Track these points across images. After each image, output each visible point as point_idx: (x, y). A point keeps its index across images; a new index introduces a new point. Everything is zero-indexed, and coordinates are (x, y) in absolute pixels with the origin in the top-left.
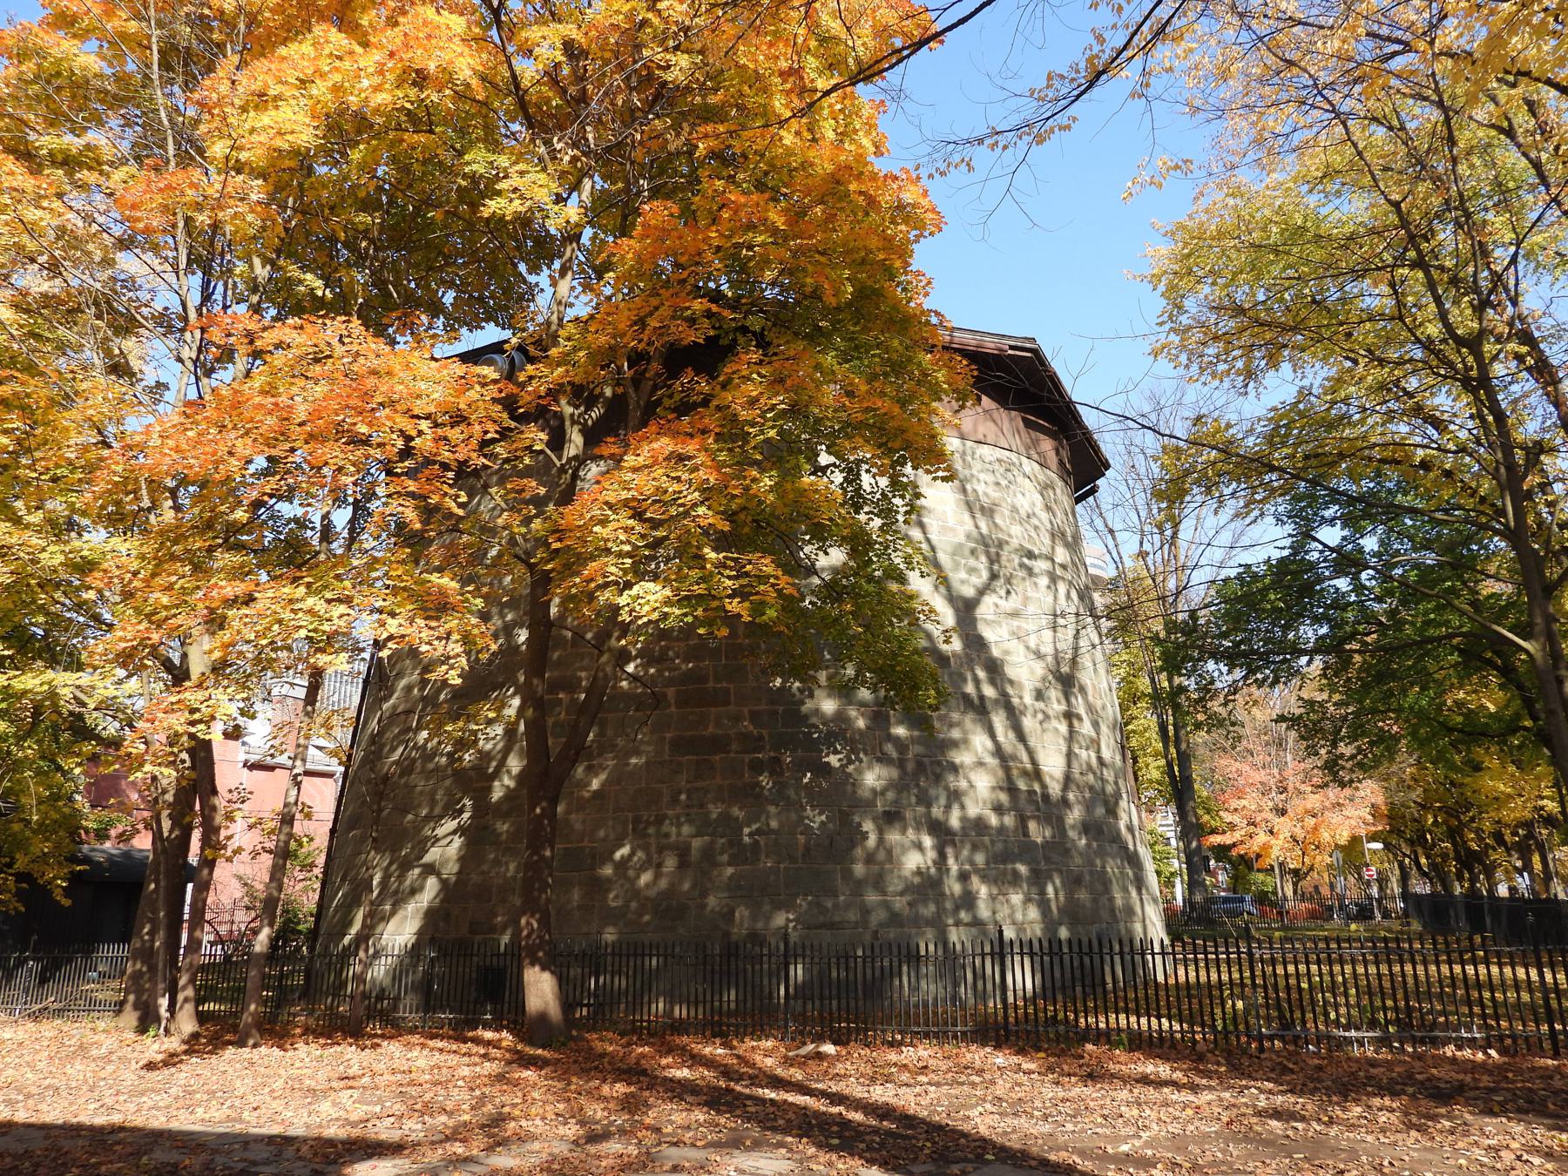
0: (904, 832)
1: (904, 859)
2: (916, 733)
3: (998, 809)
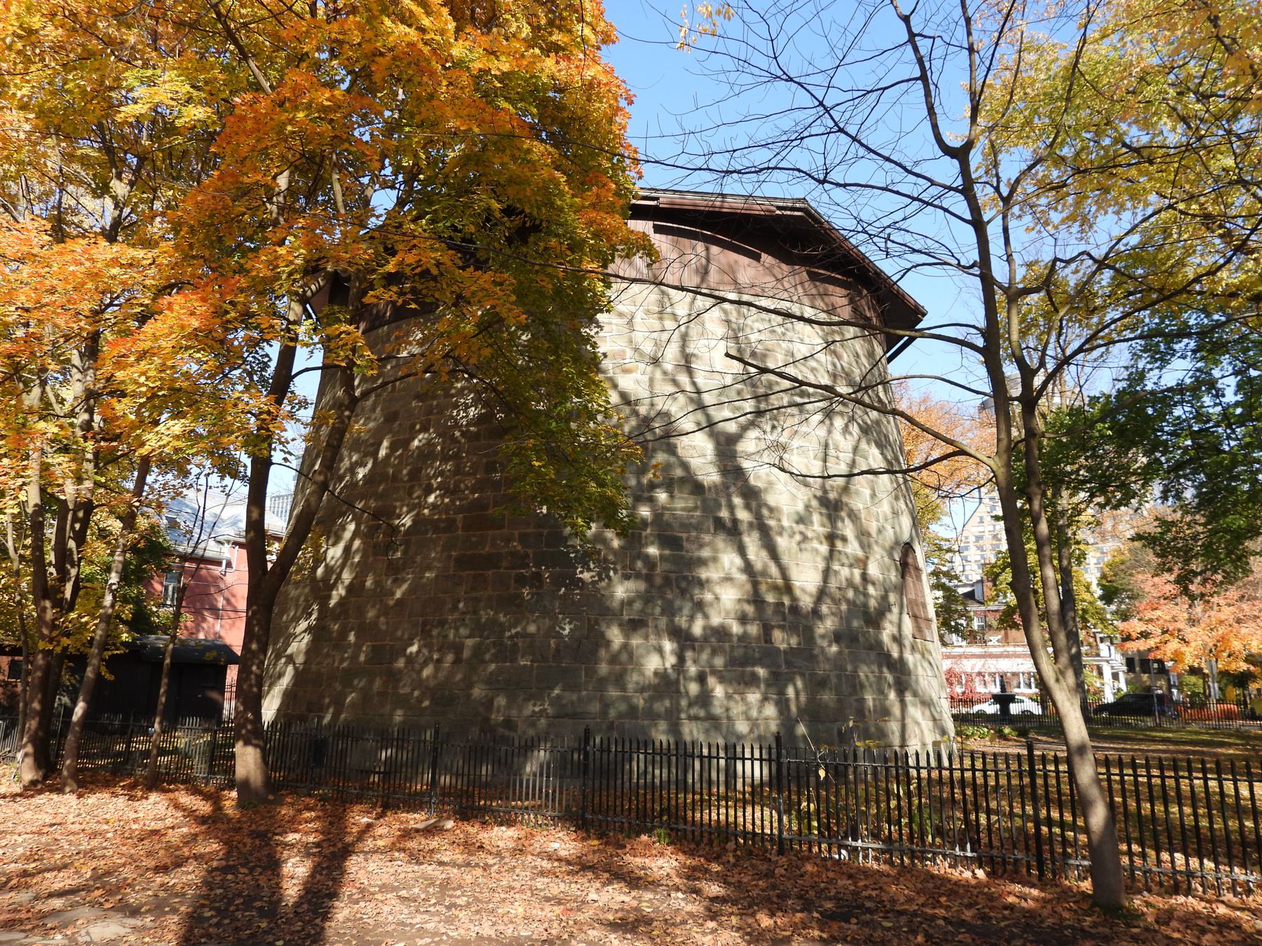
0: (646, 638)
1: (643, 661)
2: (667, 552)
3: (743, 619)
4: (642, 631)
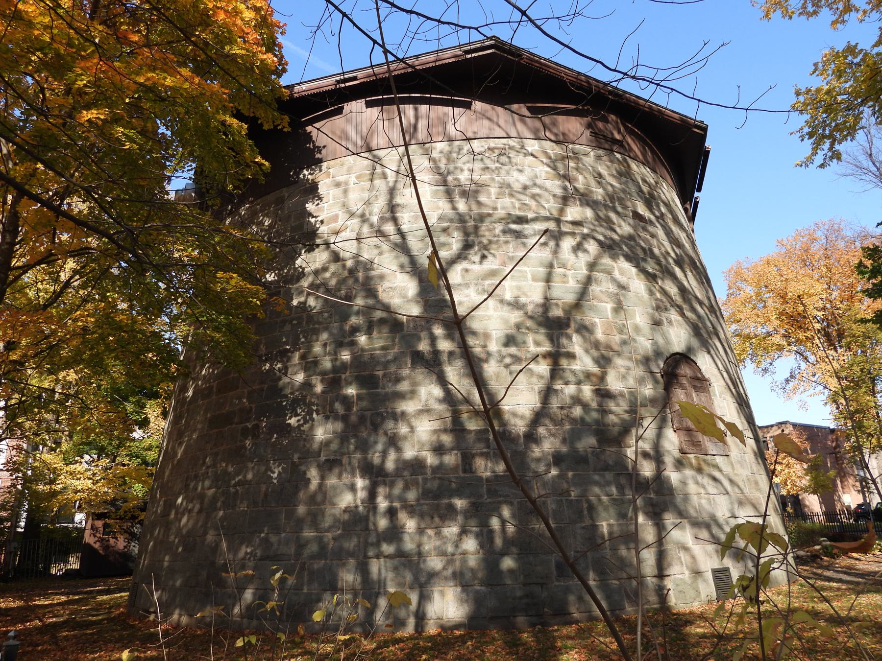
0: (340, 476)
2: (364, 391)
4: (336, 471)
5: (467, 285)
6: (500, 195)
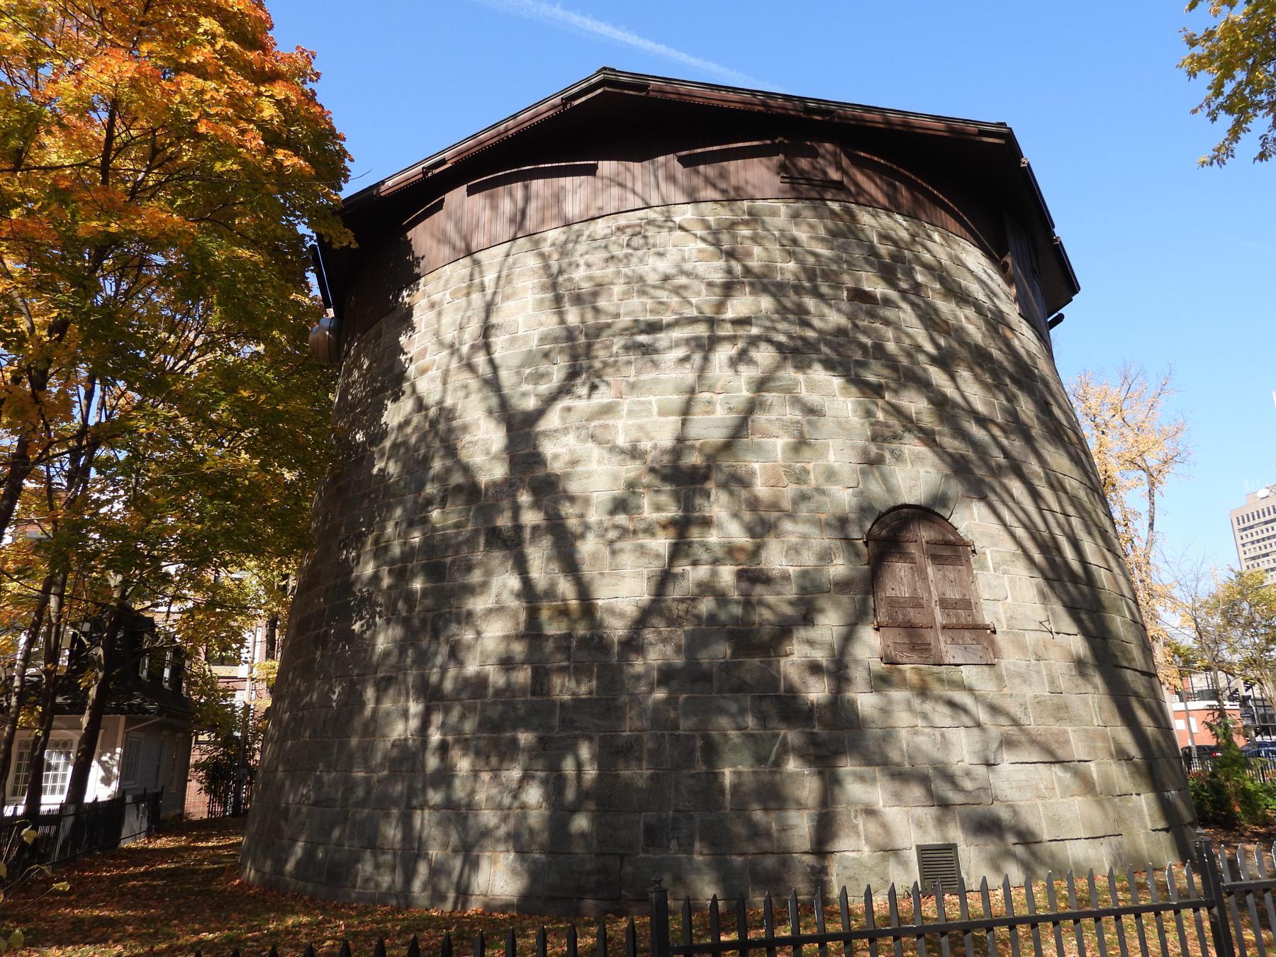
5: (566, 430)
6: (626, 295)
